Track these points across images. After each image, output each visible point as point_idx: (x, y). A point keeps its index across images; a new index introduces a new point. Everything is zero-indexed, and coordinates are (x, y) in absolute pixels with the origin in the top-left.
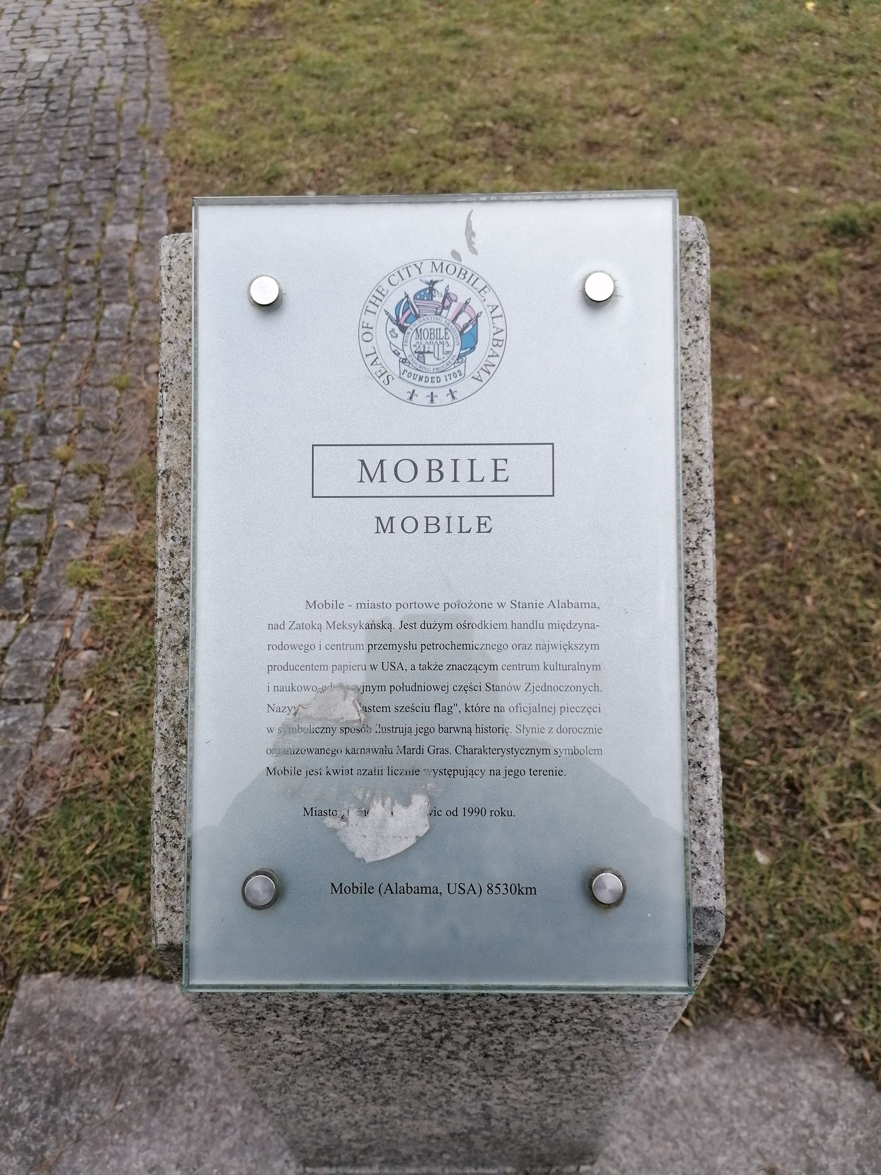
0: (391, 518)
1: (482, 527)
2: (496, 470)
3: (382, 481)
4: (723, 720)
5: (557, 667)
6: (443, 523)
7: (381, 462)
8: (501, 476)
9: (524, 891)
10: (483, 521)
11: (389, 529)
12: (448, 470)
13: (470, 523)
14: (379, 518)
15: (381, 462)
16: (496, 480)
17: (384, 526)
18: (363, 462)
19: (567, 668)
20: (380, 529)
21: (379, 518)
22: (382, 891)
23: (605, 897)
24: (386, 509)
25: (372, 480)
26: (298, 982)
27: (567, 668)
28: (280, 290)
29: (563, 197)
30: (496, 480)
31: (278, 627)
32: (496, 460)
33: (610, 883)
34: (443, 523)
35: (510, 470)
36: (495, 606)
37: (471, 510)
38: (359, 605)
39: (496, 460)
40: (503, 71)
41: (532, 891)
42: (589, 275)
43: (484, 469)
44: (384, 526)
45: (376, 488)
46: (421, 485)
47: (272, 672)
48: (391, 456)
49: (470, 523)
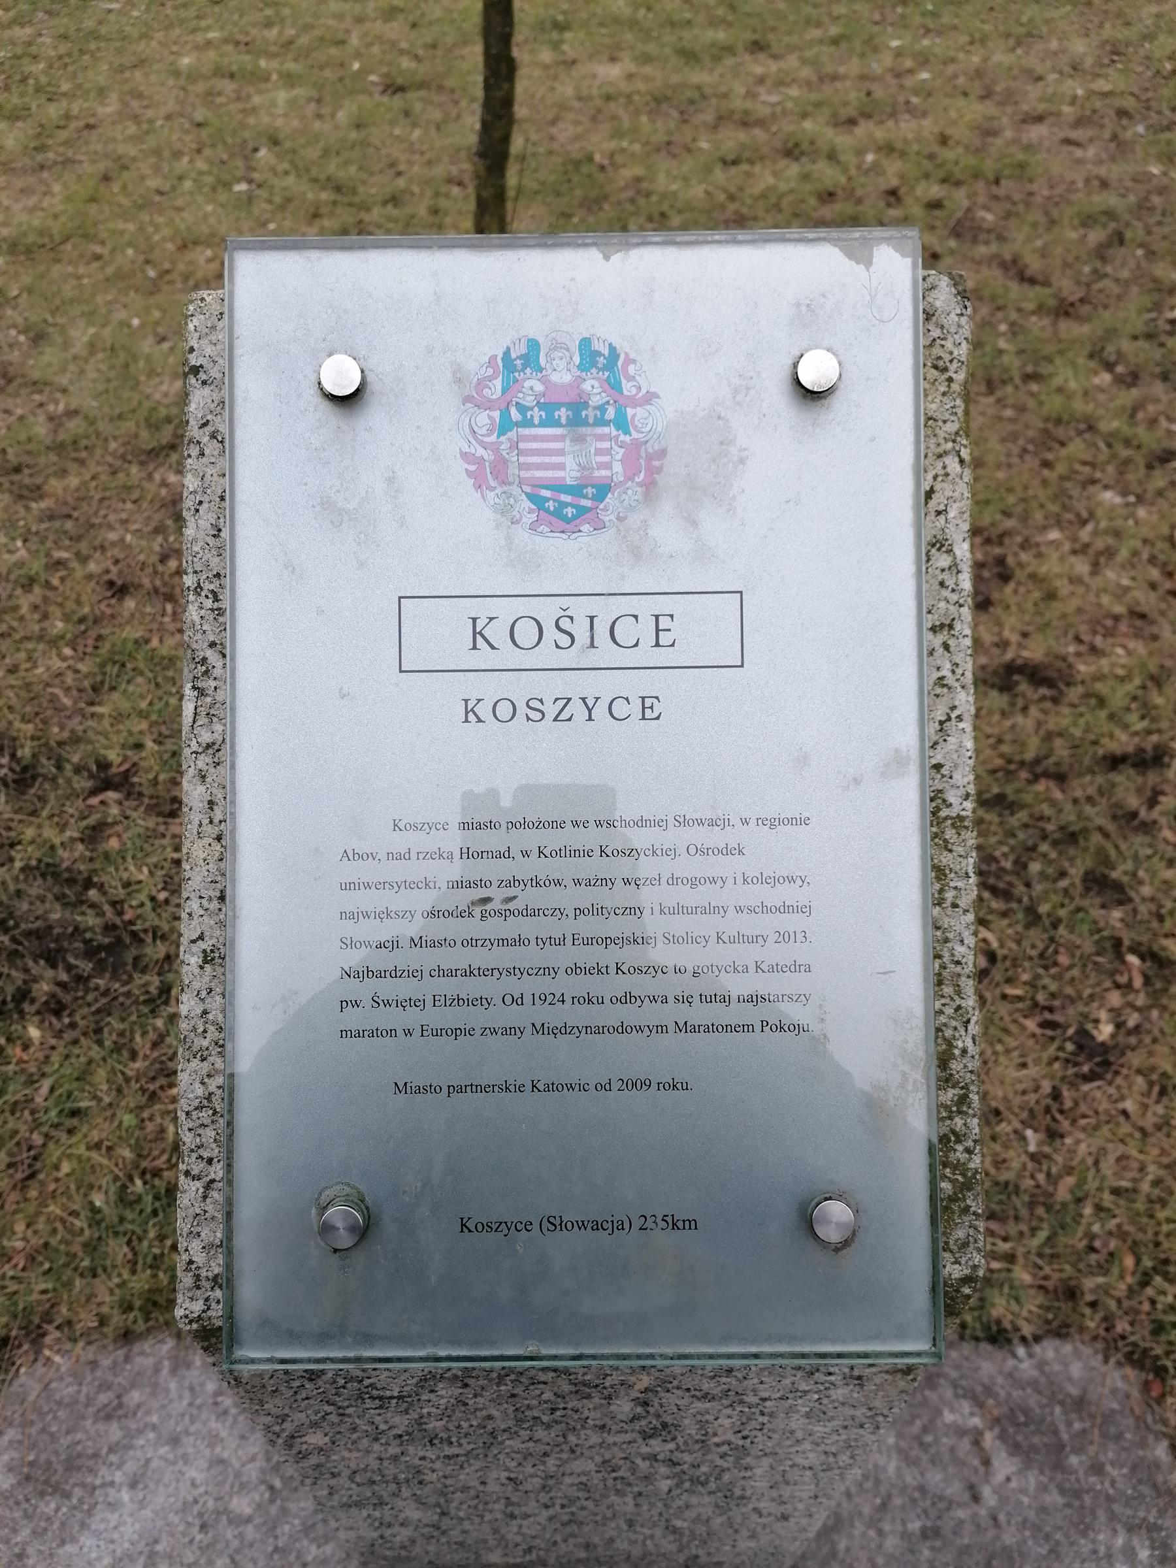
1: (648, 712)
2: (658, 630)
5: (679, 910)
8: (665, 638)
9: (680, 1224)
10: (648, 703)
12: (580, 630)
16: (657, 645)
19: (693, 911)
23: (831, 1234)
26: (571, 1351)
27: (693, 911)
29: (658, 239)
30: (657, 645)
31: (401, 857)
32: (657, 617)
33: (837, 1212)
35: (675, 630)
36: (569, 825)
37: (635, 685)
39: (657, 617)
40: (50, 67)
41: (692, 1224)
42: (795, 366)
46: (546, 655)
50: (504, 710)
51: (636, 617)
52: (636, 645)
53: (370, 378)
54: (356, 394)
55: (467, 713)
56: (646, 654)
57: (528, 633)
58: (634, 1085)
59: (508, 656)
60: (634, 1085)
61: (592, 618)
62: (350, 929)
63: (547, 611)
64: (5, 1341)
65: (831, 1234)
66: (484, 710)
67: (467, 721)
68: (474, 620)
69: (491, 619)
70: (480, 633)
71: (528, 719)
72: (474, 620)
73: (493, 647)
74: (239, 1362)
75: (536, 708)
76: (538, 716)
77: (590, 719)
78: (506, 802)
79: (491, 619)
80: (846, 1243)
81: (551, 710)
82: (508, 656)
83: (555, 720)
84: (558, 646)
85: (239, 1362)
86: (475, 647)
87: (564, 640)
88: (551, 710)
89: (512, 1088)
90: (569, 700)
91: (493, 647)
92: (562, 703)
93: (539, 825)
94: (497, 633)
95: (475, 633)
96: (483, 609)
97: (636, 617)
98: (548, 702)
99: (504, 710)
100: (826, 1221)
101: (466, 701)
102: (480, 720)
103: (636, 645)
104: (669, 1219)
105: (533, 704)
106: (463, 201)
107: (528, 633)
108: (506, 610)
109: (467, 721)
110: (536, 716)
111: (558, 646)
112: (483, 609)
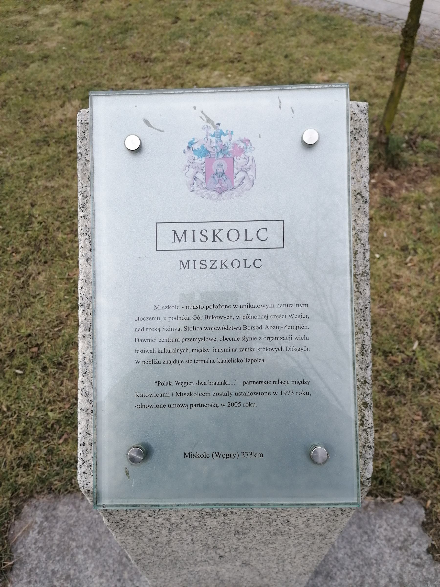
0: (188, 261)
3: (185, 241)
4: (69, 385)
6: (198, 265)
7: (185, 231)
9: (257, 455)
11: (187, 267)
13: (250, 263)
14: (181, 261)
15: (185, 231)
17: (184, 265)
18: (175, 232)
20: (182, 267)
21: (181, 261)
22: (237, 455)
24: (185, 256)
25: (180, 241)
28: (319, 139)
34: (198, 265)
38: (187, 307)
42: (302, 136)
43: (210, 235)
44: (184, 265)
45: (182, 246)
46: (240, 243)
47: (184, 342)
48: (189, 228)
49: (250, 263)
50: (236, 264)
51: (266, 229)
52: (267, 240)
53: (143, 142)
54: (141, 146)
55: (222, 265)
58: (234, 404)
59: (226, 244)
60: (234, 404)
62: (141, 346)
63: (241, 227)
66: (228, 264)
67: (222, 268)
68: (214, 230)
69: (220, 230)
70: (216, 235)
71: (201, 268)
72: (214, 230)
73: (221, 241)
75: (203, 264)
76: (204, 267)
77: (195, 268)
78: (197, 297)
79: (220, 230)
81: (209, 265)
82: (226, 244)
83: (211, 268)
84: (201, 241)
86: (214, 241)
87: (204, 239)
88: (209, 265)
89: (305, 393)
90: (216, 261)
91: (221, 241)
92: (213, 262)
93: (220, 307)
94: (222, 235)
97: (266, 229)
98: (208, 261)
99: (236, 264)
101: (222, 261)
102: (227, 268)
104: (253, 454)
105: (202, 262)
108: (226, 227)
109: (222, 268)
110: (203, 267)
111: (201, 241)
112: (217, 226)
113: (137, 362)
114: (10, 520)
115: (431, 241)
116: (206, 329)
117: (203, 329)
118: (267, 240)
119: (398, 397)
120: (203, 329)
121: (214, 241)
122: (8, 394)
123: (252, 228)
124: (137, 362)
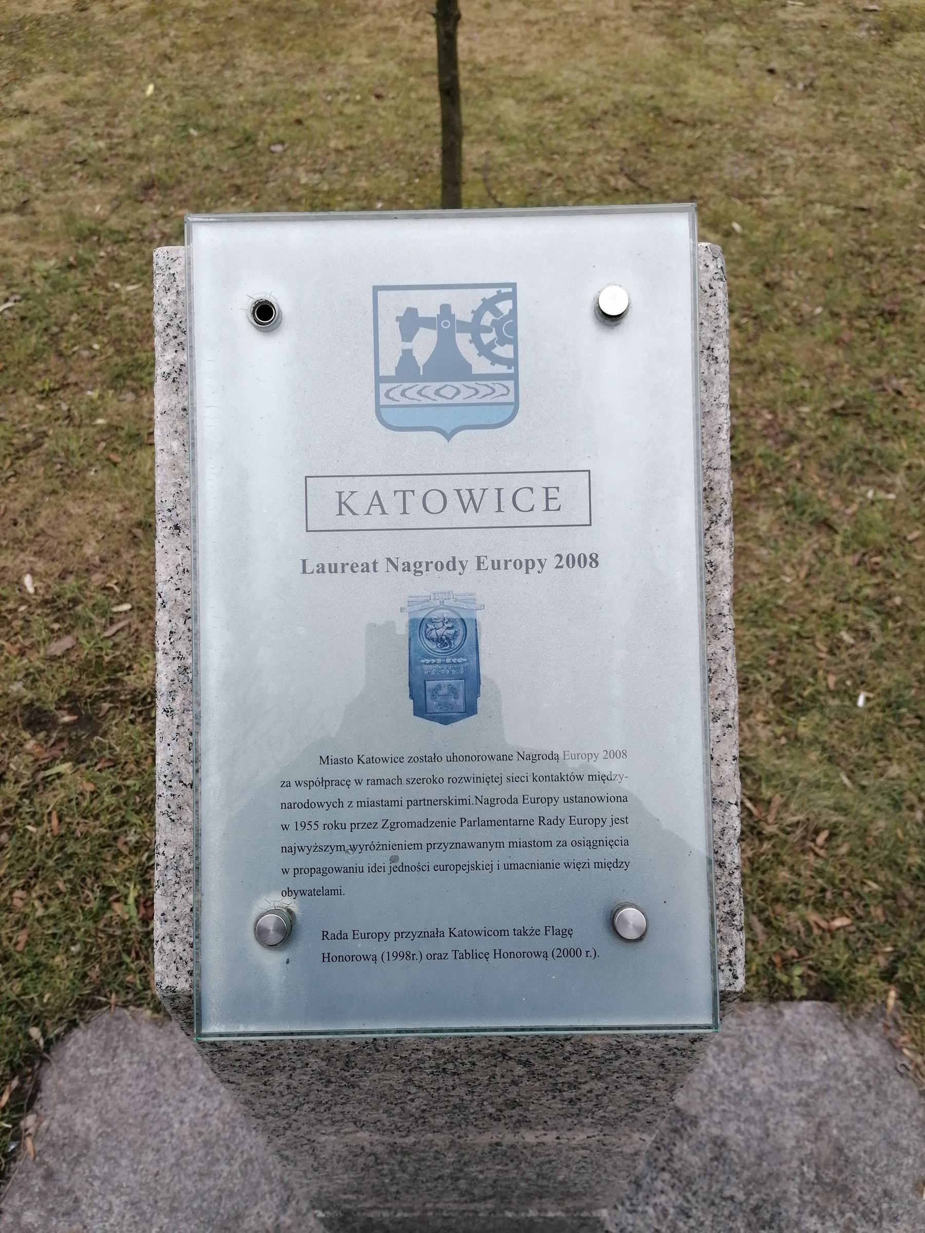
2: (547, 499)
16: (547, 509)
30: (547, 509)
32: (547, 489)
39: (547, 489)
51: (531, 489)
56: (539, 517)
57: (435, 502)
58: (569, 953)
60: (569, 953)
61: (499, 490)
64: (921, 938)
65: (631, 933)
68: (340, 493)
69: (353, 493)
72: (340, 493)
73: (354, 514)
74: (206, 1035)
79: (353, 493)
80: (640, 939)
85: (206, 1035)
86: (340, 514)
91: (354, 514)
94: (359, 503)
95: (340, 503)
96: (346, 485)
97: (531, 489)
100: (625, 922)
103: (532, 509)
106: (433, 187)
107: (435, 502)
112: (346, 485)
113: (285, 871)
114: (510, 1202)
115: (43, 531)
116: (298, 784)
117: (293, 784)
118: (532, 509)
119: (910, 434)
120: (293, 784)
121: (340, 514)
122: (747, 596)
123: (368, 487)
124: (285, 871)
